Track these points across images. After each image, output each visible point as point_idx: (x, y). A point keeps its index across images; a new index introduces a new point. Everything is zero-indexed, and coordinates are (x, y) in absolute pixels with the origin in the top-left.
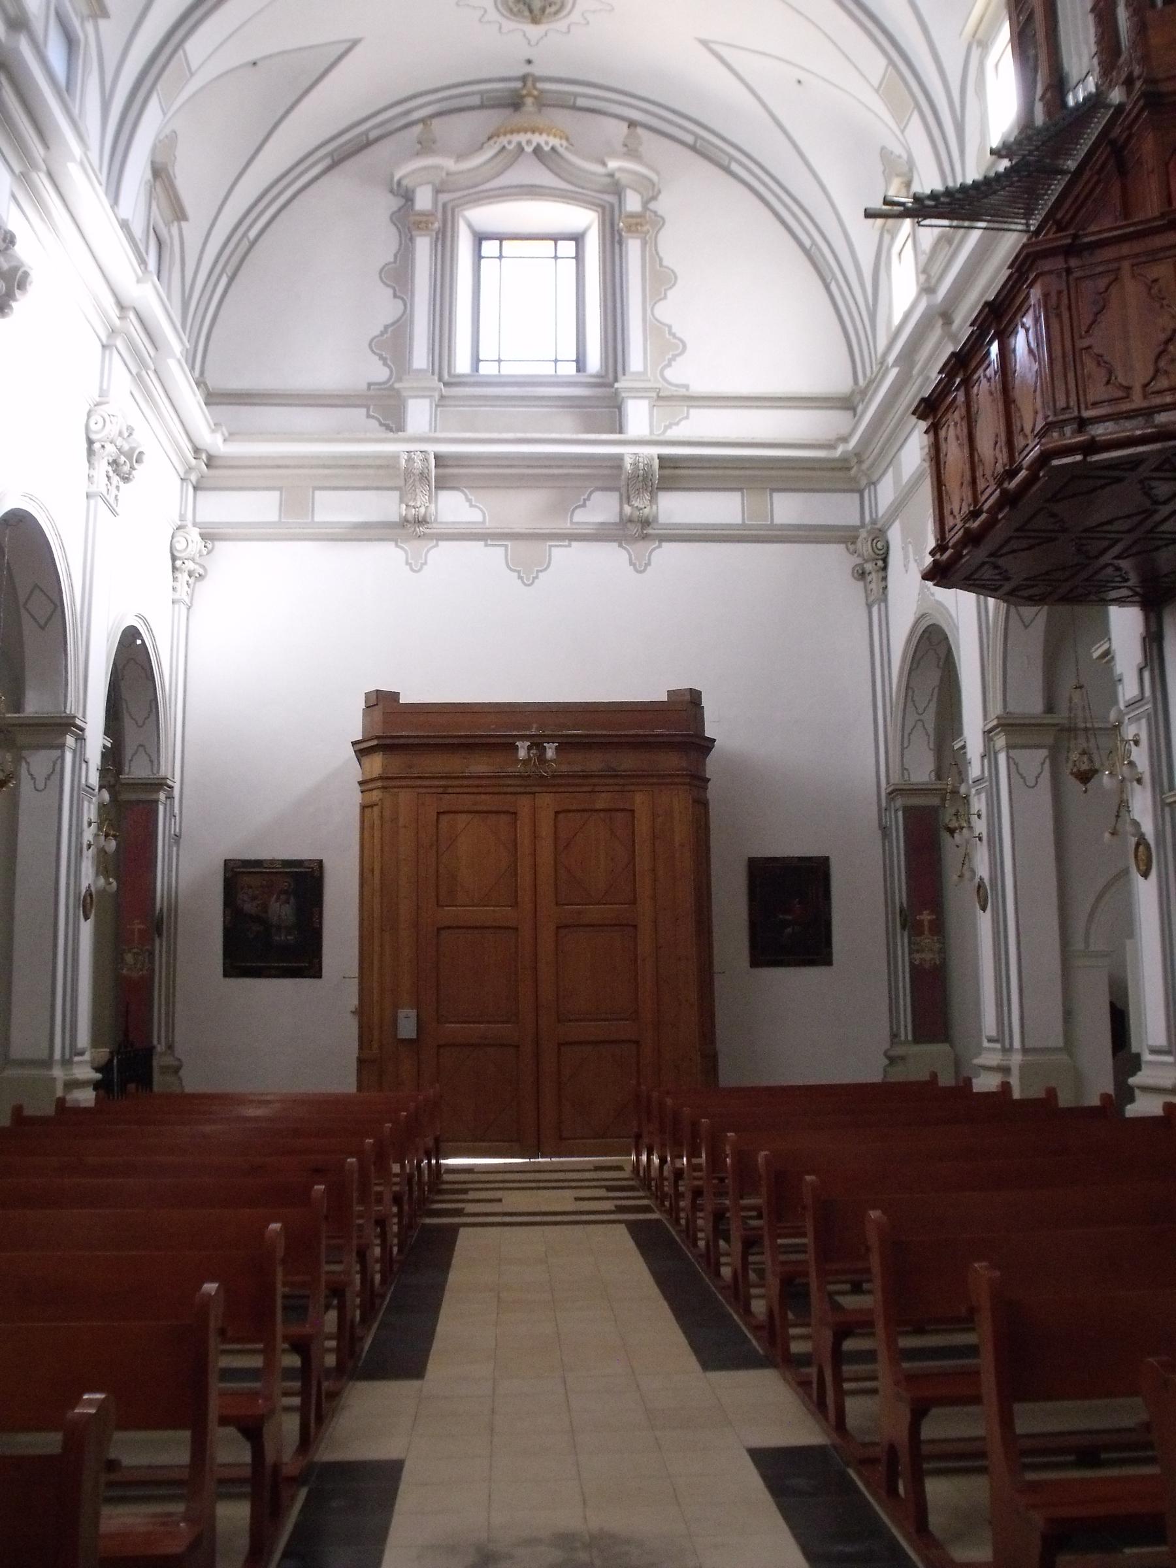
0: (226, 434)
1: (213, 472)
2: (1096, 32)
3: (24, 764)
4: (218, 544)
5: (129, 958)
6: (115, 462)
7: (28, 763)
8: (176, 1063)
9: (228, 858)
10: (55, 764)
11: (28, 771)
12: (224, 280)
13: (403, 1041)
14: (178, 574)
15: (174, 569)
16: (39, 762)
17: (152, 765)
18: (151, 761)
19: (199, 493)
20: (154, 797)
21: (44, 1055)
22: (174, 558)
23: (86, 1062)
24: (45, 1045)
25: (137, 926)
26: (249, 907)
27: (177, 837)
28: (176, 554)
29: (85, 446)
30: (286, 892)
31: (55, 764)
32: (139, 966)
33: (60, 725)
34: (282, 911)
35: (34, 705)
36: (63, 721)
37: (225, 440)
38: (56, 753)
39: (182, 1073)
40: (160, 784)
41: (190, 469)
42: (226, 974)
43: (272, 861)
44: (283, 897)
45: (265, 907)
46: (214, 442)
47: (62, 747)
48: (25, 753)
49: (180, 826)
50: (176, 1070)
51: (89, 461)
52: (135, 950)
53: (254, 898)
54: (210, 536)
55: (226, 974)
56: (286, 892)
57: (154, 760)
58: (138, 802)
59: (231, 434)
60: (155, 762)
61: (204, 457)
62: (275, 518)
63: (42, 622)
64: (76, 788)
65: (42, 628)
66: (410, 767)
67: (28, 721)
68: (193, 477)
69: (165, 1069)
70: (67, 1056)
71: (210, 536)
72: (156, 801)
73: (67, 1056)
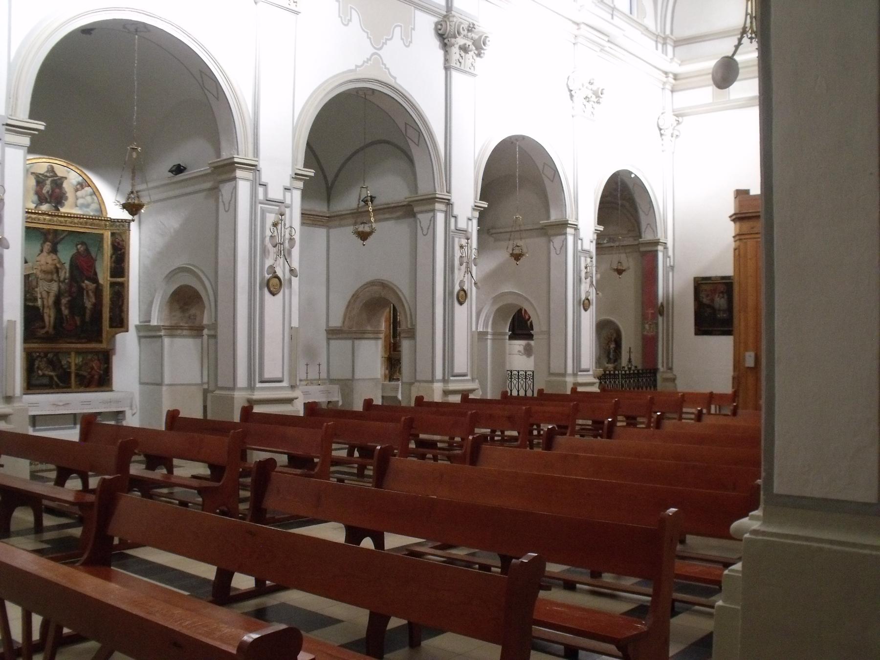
0: (679, 62)
1: (678, 82)
2: (65, 189)
3: (551, 243)
4: (685, 118)
5: (647, 326)
6: (586, 98)
7: (553, 242)
8: (674, 377)
9: (696, 276)
10: (563, 241)
11: (553, 245)
12: (697, 607)
13: (748, 368)
14: (663, 137)
15: (661, 135)
16: (557, 241)
17: (654, 233)
18: (654, 231)
19: (675, 94)
20: (655, 249)
21: (563, 371)
22: (660, 129)
23: (591, 375)
24: (563, 366)
25: (651, 311)
26: (705, 300)
27: (672, 267)
28: (661, 127)
29: (569, 93)
30: (722, 292)
31: (563, 241)
32: (651, 329)
33: (563, 224)
34: (720, 302)
35: (554, 217)
36: (564, 222)
37: (680, 65)
38: (563, 237)
39: (677, 382)
40: (656, 243)
41: (664, 83)
42: (697, 334)
43: (716, 277)
44: (721, 295)
45: (712, 300)
46: (675, 68)
47: (565, 234)
48: (552, 238)
49: (674, 261)
50: (673, 380)
51: (572, 100)
52: (650, 323)
53: (707, 296)
54: (679, 115)
55: (697, 334)
56: (722, 292)
57: (655, 231)
58: (650, 251)
59: (682, 61)
60: (655, 232)
61: (671, 76)
62: (711, 101)
63: (552, 179)
64: (576, 251)
65: (552, 181)
66: (752, 228)
67: (552, 224)
68: (668, 87)
69: (666, 380)
70: (575, 372)
71: (679, 115)
72: (657, 251)
73: (575, 372)
